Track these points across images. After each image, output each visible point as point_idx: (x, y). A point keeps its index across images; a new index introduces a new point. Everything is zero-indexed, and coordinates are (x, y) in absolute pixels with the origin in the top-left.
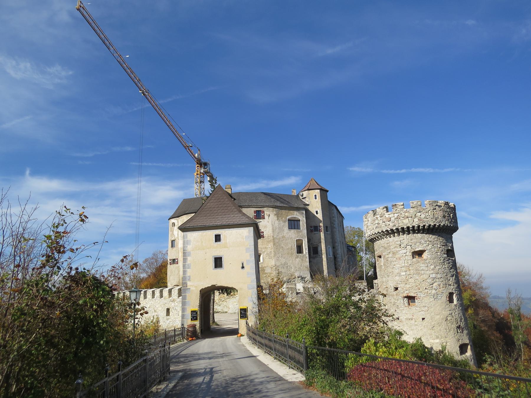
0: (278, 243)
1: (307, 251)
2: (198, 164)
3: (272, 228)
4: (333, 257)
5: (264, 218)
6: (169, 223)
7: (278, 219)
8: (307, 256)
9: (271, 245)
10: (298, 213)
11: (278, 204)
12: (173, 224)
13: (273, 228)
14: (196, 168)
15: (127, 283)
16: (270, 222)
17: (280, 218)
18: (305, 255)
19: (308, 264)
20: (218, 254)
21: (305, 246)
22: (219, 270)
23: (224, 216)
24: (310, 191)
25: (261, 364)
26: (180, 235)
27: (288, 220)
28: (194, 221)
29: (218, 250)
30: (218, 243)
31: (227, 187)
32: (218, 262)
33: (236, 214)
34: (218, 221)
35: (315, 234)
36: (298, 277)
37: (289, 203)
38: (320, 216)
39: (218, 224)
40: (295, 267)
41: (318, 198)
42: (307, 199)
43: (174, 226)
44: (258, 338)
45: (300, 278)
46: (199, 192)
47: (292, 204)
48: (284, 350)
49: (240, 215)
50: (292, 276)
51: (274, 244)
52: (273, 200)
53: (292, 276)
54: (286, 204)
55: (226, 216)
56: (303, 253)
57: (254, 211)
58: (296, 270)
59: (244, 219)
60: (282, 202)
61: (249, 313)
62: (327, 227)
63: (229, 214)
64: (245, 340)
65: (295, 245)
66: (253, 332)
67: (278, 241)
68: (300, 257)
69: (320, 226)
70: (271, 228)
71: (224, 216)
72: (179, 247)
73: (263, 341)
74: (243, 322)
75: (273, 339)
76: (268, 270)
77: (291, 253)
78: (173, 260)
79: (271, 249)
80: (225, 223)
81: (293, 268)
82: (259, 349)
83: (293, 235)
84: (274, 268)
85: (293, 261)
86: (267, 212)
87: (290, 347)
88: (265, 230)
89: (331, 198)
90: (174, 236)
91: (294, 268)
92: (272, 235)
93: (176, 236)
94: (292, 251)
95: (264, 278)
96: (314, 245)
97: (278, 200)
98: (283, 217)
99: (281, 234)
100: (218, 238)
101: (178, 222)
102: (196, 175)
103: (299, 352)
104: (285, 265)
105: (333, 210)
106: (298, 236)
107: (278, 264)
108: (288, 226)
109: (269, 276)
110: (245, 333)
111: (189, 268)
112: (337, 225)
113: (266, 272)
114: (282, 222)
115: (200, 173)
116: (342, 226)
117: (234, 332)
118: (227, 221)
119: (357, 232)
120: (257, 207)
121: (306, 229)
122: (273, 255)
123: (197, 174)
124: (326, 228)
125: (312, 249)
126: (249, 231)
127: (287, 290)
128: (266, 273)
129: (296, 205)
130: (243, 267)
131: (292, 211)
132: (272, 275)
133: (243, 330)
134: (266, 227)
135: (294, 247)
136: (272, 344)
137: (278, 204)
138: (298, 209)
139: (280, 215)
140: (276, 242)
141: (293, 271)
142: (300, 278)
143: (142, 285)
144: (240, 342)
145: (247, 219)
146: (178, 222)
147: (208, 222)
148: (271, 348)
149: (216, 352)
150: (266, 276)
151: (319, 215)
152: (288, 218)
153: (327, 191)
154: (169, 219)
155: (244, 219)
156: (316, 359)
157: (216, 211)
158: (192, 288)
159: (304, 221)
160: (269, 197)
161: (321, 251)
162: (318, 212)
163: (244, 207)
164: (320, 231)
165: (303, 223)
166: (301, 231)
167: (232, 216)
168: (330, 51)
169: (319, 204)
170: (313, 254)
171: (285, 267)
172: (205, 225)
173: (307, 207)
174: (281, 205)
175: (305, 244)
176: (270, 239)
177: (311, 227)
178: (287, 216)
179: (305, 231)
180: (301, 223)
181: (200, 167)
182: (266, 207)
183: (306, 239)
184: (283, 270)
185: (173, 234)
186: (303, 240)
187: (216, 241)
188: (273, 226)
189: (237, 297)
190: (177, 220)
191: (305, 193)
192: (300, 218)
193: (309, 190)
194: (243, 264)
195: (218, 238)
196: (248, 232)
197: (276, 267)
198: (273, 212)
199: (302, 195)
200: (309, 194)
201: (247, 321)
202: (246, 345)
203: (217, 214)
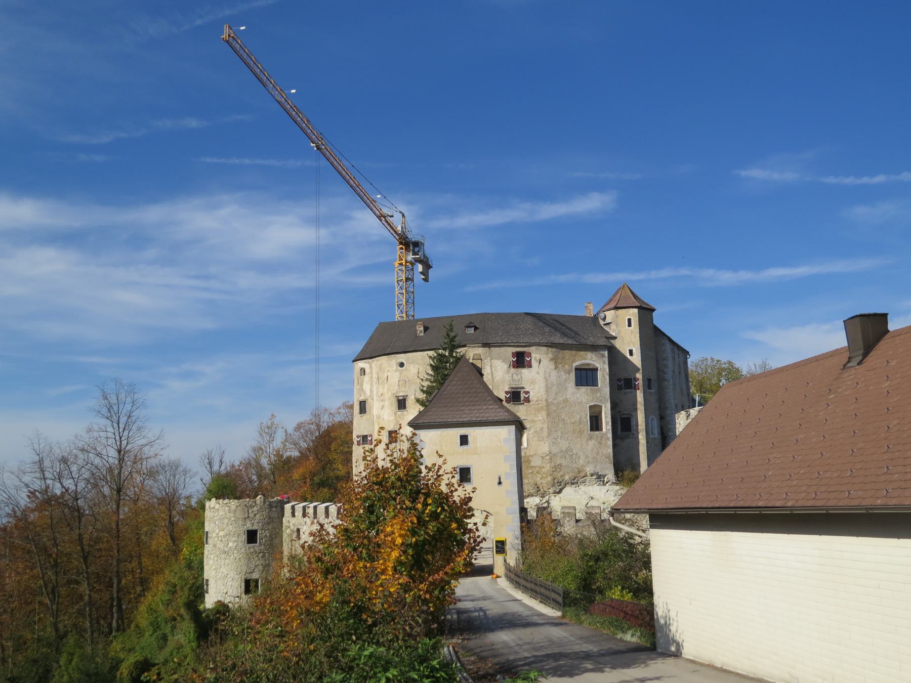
0: (555, 411)
1: (610, 427)
2: (401, 243)
3: (544, 384)
4: (660, 437)
5: (531, 366)
6: (353, 367)
7: (556, 368)
8: (610, 435)
9: (542, 416)
10: (594, 356)
11: (558, 339)
12: (362, 371)
13: (547, 384)
14: (399, 252)
15: (262, 468)
16: (541, 374)
17: (560, 366)
18: (606, 434)
19: (610, 450)
20: (464, 463)
21: (606, 417)
23: (473, 408)
24: (620, 310)
25: (525, 606)
26: (375, 393)
27: (576, 369)
28: (429, 414)
30: (465, 447)
31: (475, 358)
33: (490, 405)
34: (464, 416)
36: (592, 475)
37: (578, 334)
38: (636, 360)
39: (465, 420)
40: (587, 457)
41: (635, 324)
42: (613, 326)
43: (363, 374)
44: (522, 582)
45: (595, 477)
46: (404, 300)
47: (583, 338)
48: (548, 593)
49: (496, 406)
50: (579, 472)
51: (548, 415)
52: (547, 329)
53: (579, 472)
54: (572, 338)
55: (476, 407)
56: (602, 430)
57: (513, 353)
58: (589, 462)
59: (501, 414)
60: (564, 334)
61: (508, 547)
62: (649, 380)
63: (480, 405)
64: (503, 583)
65: (586, 415)
66: (515, 574)
67: (555, 408)
68: (595, 437)
69: (636, 379)
70: (543, 385)
71: (473, 408)
72: (375, 414)
73: (528, 585)
74: (499, 558)
75: (538, 583)
76: (536, 462)
77: (580, 431)
78: (363, 436)
79: (543, 423)
80: (474, 419)
81: (583, 458)
82: (524, 594)
83: (584, 397)
84: (548, 457)
85: (582, 445)
86: (537, 355)
87: (553, 591)
88: (532, 387)
89: (658, 320)
90: (365, 393)
91: (584, 458)
92: (545, 397)
93: (368, 393)
94: (582, 426)
95: (530, 476)
96: (624, 414)
97: (556, 329)
98: (565, 364)
99: (562, 396)
100: (464, 440)
101: (371, 367)
102: (397, 265)
103: (559, 594)
104: (567, 454)
105: (664, 345)
106: (593, 398)
107: (555, 450)
108: (574, 379)
109: (538, 472)
110: (503, 573)
112: (671, 373)
113: (532, 464)
114: (563, 373)
115: (406, 262)
116: (682, 371)
117: (487, 571)
118: (477, 415)
119: (723, 369)
120: (518, 346)
121: (608, 386)
122: (545, 434)
123: (401, 264)
124: (648, 383)
125: (619, 422)
127: (562, 516)
128: (533, 467)
129: (591, 340)
130: (500, 483)
131: (582, 353)
132: (543, 470)
133: (499, 569)
134: (533, 382)
135: (585, 420)
136: (538, 589)
137: (558, 339)
138: (594, 348)
139: (560, 361)
140: (552, 411)
141: (581, 463)
142: (595, 477)
143: (295, 474)
144: (498, 585)
145: (506, 414)
146: (371, 367)
147: (450, 416)
148: (536, 592)
149: (474, 595)
150: (532, 473)
151: (634, 356)
152: (574, 365)
153: (653, 310)
154: (354, 361)
155: (501, 414)
156: (581, 603)
157: (460, 400)
159: (604, 370)
160: (541, 324)
161: (637, 425)
162: (634, 351)
163: (493, 346)
164: (636, 388)
165: (603, 374)
166: (599, 390)
167: (484, 407)
169: (635, 337)
170: (622, 431)
171: (567, 456)
172: (445, 420)
173: (612, 341)
174: (562, 341)
175: (606, 414)
176: (540, 405)
177: (619, 380)
178: (574, 361)
179: (607, 390)
180: (599, 374)
181: (406, 249)
182: (535, 345)
183: (609, 405)
184: (564, 463)
185: (363, 390)
186: (601, 407)
187: (461, 444)
188: (547, 380)
190: (369, 363)
191: (610, 315)
192: (598, 365)
193: (616, 308)
194: (500, 478)
195: (464, 440)
196: (507, 432)
197: (552, 456)
198: (547, 354)
199: (604, 319)
200: (617, 316)
201: (505, 558)
202: (507, 589)
203: (462, 404)
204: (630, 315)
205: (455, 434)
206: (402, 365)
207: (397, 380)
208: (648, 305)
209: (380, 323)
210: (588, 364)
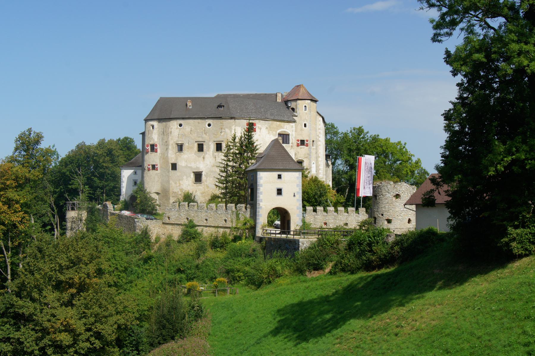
20: (279, 187)
22: (280, 197)
29: (279, 184)
32: (279, 192)
35: (301, 148)
100: (280, 177)
111: (262, 194)
114: (272, 136)
126: (299, 174)
130: (294, 196)
158: (263, 207)
162: (307, 125)
168: (388, 270)
178: (278, 129)
189: (411, 218)
195: (280, 177)
204: (306, 104)
205: (276, 174)
206: (181, 125)
207: (177, 134)
208: (314, 98)
209: (161, 98)
210: (285, 132)
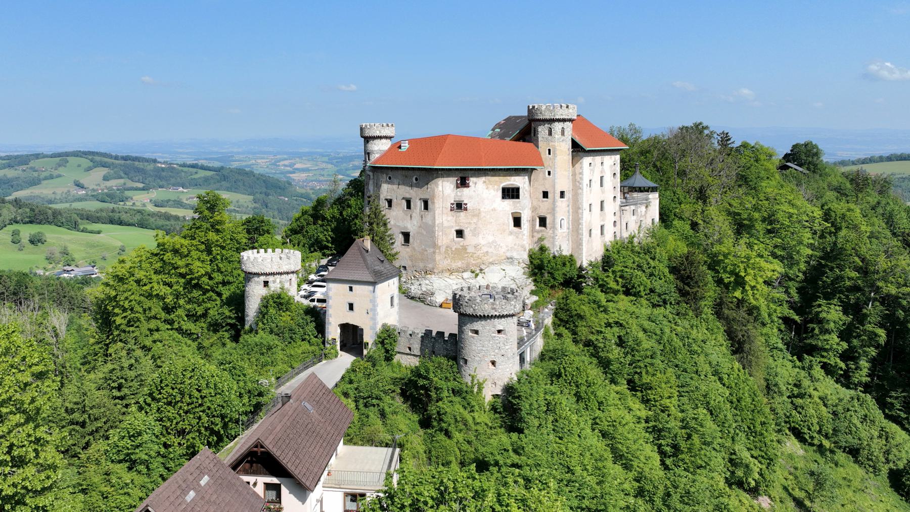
40: (507, 246)
